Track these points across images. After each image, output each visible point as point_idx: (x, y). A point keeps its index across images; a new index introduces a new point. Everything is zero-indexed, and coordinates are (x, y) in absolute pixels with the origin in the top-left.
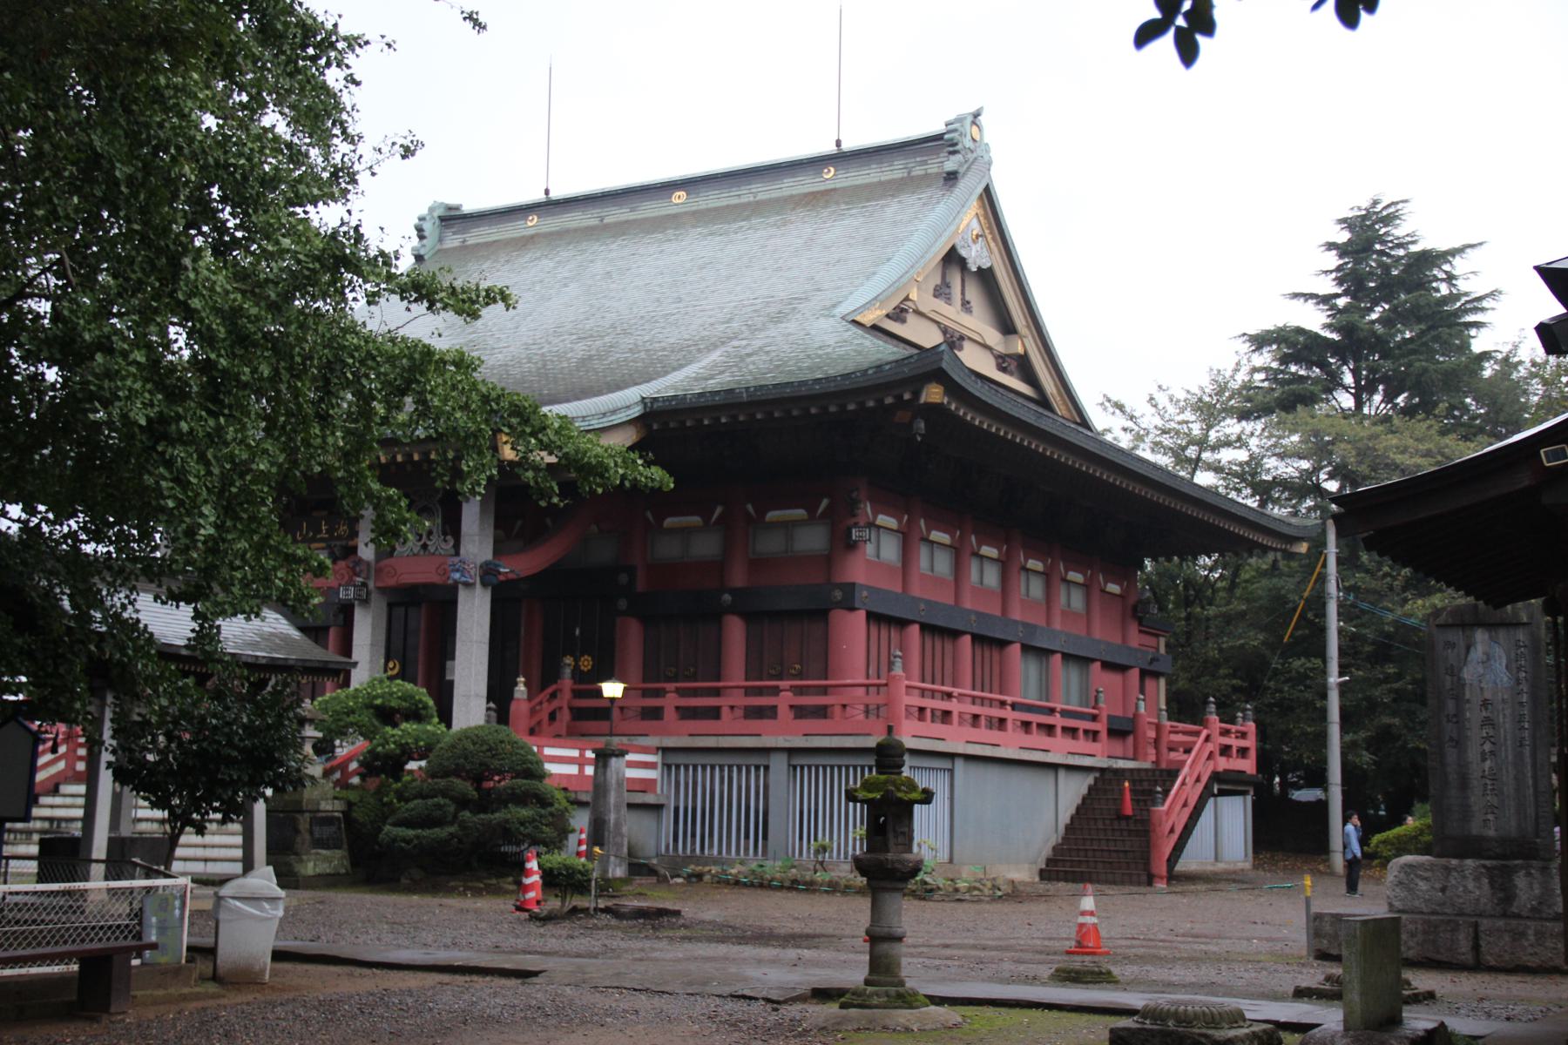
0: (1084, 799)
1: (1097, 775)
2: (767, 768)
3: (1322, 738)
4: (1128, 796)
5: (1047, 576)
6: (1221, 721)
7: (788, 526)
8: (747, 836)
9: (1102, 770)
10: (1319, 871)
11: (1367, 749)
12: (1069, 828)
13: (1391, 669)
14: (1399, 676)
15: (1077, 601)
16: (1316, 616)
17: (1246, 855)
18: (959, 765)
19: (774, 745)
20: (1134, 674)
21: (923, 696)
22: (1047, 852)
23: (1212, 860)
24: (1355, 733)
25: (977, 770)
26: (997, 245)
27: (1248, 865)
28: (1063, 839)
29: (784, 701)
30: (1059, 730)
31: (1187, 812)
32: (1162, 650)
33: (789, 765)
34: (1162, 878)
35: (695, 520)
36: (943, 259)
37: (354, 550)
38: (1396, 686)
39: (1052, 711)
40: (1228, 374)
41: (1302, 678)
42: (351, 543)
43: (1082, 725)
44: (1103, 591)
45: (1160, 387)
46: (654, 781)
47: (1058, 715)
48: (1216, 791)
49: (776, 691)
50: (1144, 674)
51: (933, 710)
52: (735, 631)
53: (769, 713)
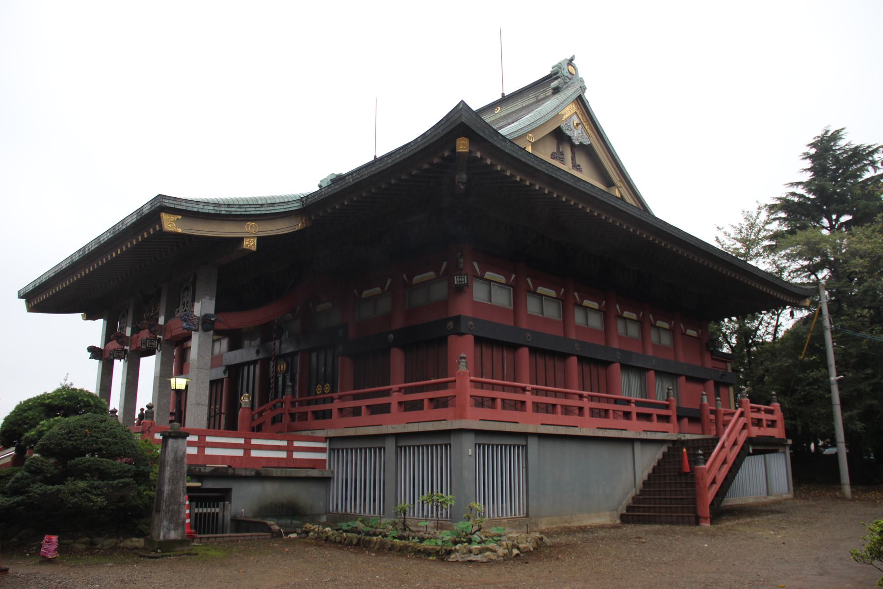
0: (659, 462)
1: (671, 445)
2: (384, 448)
3: (830, 417)
4: (686, 458)
5: (641, 322)
6: (751, 403)
7: (427, 284)
8: (374, 501)
10: (836, 497)
11: (859, 420)
12: (645, 483)
13: (869, 371)
14: (874, 376)
15: (666, 340)
16: (821, 345)
17: (789, 489)
18: (533, 444)
20: (711, 384)
21: (592, 401)
22: (627, 500)
23: (765, 494)
24: (850, 411)
25: (550, 448)
26: (593, 132)
27: (790, 496)
28: (641, 491)
29: (394, 399)
30: (634, 416)
31: (725, 469)
32: (730, 370)
33: (397, 447)
34: (706, 518)
38: (873, 381)
39: (628, 402)
40: (754, 215)
41: (816, 381)
43: (655, 412)
44: (684, 334)
45: (718, 228)
46: (325, 460)
47: (633, 405)
48: (751, 451)
49: (387, 393)
50: (717, 385)
51: (503, 400)
52: (397, 358)
53: (385, 409)
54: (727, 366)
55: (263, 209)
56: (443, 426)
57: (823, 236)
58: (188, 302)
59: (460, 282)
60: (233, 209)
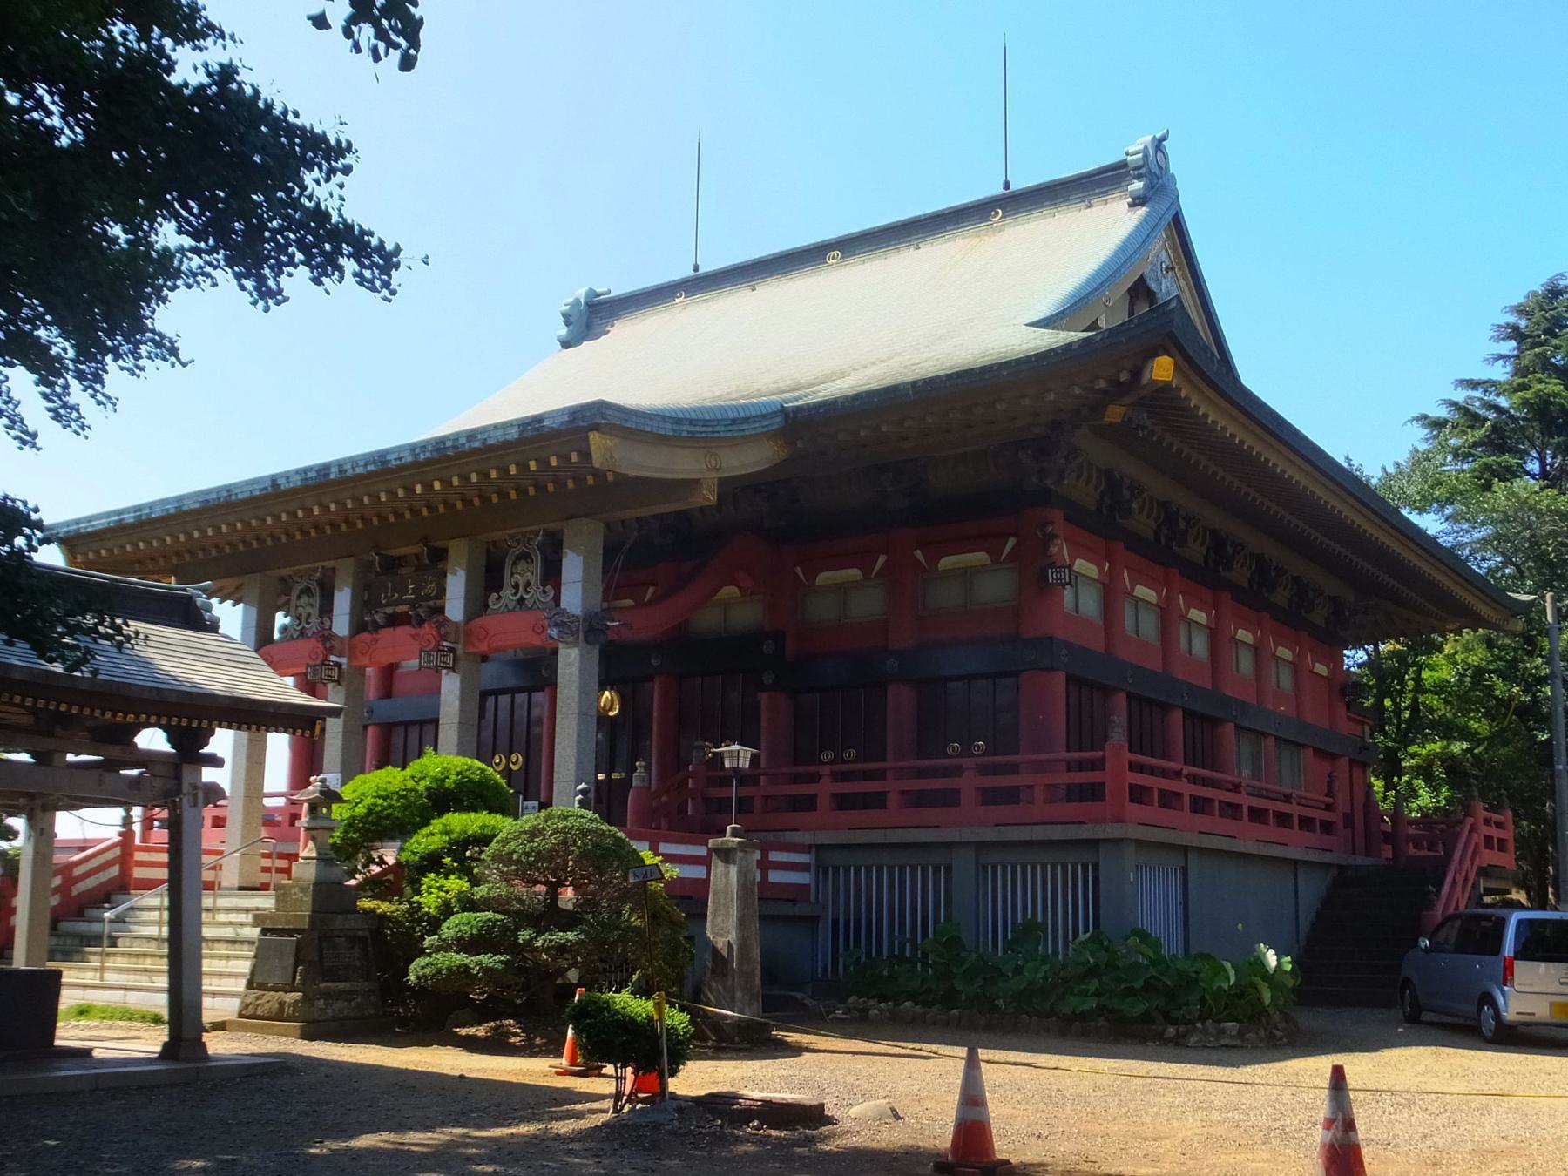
2: (949, 869)
9: (1340, 867)
19: (957, 839)
20: (1344, 763)
35: (854, 573)
36: (1129, 290)
37: (441, 610)
39: (1236, 788)
42: (439, 603)
49: (957, 771)
54: (1363, 728)
55: (735, 428)
56: (1086, 832)
57: (15, 142)
58: (528, 584)
59: (1057, 579)
60: (697, 429)
